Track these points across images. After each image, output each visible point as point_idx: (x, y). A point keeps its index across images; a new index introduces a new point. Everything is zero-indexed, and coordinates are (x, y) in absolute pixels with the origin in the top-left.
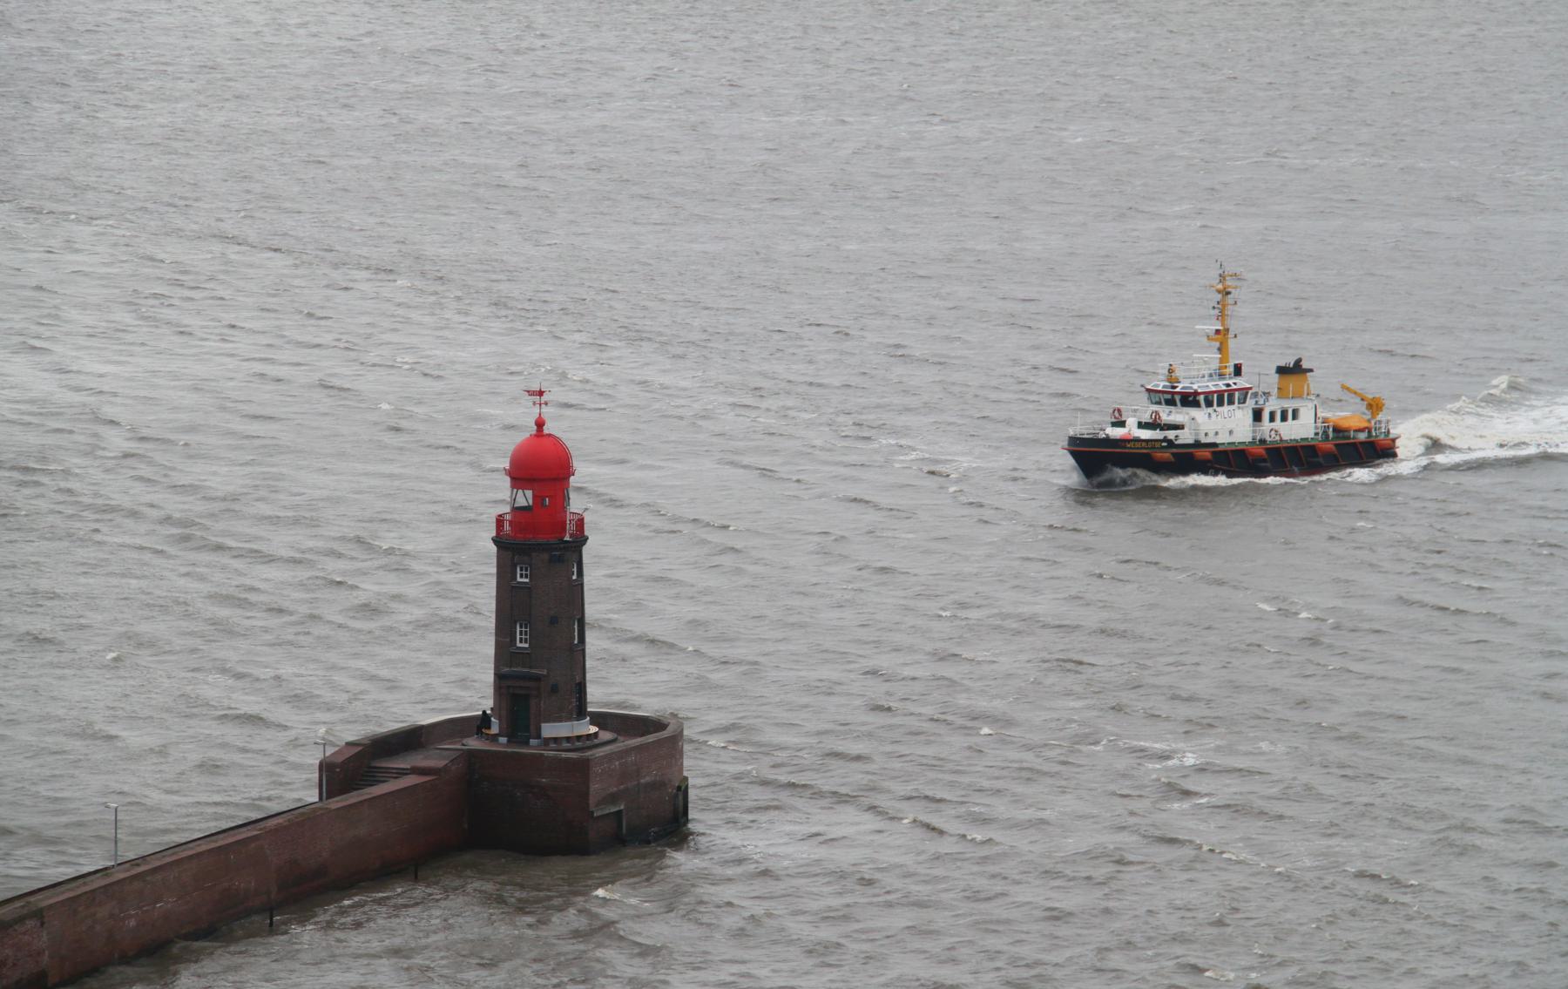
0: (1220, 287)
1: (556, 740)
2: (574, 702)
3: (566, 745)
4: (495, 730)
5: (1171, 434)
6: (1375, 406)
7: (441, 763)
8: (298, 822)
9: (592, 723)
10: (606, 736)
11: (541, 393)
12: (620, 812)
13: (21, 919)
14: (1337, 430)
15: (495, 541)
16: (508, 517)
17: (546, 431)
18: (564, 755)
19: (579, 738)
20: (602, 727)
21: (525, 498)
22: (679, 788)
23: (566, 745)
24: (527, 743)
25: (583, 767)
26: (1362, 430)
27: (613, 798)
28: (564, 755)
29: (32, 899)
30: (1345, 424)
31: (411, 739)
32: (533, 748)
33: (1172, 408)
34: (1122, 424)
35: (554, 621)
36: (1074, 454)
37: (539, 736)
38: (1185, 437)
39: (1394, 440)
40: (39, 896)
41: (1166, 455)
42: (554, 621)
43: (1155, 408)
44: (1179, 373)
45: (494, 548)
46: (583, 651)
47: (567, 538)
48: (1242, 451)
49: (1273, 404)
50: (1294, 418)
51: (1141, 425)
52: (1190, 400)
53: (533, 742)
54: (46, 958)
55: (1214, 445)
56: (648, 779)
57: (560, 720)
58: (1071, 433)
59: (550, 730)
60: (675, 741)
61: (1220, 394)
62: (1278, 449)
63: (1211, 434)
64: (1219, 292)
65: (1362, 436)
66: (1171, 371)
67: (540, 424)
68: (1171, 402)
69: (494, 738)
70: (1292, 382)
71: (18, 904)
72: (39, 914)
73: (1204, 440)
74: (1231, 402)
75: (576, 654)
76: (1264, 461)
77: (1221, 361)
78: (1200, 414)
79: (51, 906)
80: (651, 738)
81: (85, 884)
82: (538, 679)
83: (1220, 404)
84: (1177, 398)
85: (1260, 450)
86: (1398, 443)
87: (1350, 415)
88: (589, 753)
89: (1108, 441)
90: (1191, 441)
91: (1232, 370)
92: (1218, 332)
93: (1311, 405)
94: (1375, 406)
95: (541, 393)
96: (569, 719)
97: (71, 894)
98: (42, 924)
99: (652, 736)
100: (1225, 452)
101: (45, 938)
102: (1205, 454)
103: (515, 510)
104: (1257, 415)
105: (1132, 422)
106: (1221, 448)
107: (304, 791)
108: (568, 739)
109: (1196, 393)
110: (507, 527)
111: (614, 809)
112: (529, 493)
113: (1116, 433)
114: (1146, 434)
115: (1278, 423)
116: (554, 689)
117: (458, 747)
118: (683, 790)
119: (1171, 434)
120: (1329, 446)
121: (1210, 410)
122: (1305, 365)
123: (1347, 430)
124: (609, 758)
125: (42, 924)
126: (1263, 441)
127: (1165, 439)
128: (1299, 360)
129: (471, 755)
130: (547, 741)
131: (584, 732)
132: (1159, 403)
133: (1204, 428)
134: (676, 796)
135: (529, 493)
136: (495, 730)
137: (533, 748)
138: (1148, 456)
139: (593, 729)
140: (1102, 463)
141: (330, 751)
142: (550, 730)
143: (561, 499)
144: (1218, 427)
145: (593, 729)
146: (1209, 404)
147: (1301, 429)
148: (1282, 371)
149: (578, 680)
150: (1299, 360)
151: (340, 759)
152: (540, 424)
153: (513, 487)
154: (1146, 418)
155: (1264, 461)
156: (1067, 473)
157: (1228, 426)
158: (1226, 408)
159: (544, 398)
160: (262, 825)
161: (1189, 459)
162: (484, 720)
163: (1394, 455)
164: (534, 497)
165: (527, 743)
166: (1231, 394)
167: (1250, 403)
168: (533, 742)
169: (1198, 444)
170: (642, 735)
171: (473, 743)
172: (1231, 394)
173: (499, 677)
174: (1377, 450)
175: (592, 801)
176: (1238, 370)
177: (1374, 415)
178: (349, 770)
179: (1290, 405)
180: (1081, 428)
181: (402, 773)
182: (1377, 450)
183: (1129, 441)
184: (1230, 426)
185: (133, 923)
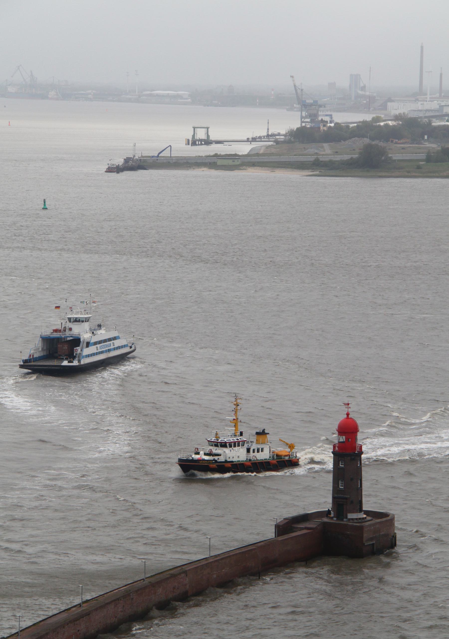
0: (235, 403)
1: (352, 519)
2: (358, 507)
3: (356, 521)
4: (332, 515)
5: (216, 458)
6: (291, 447)
7: (314, 526)
8: (266, 545)
9: (364, 514)
10: (369, 518)
11: (348, 404)
12: (373, 544)
13: (180, 574)
14: (277, 455)
15: (333, 453)
16: (337, 445)
17: (350, 416)
18: (355, 524)
19: (360, 519)
20: (367, 515)
21: (343, 439)
22: (393, 536)
23: (356, 521)
24: (342, 520)
25: (361, 529)
26: (286, 456)
27: (372, 539)
28: (355, 524)
29: (183, 567)
30: (280, 454)
31: (304, 518)
32: (345, 522)
33: (217, 448)
34: (198, 453)
35: (352, 480)
36: (180, 465)
37: (347, 518)
38: (222, 459)
39: (298, 459)
40: (186, 566)
41: (214, 466)
42: (352, 480)
43: (211, 448)
44: (219, 435)
45: (332, 455)
46: (361, 490)
47: (356, 452)
48: (243, 464)
49: (254, 446)
50: (262, 451)
51: (205, 454)
52: (224, 445)
53: (345, 520)
54: (188, 587)
55: (232, 462)
56: (383, 533)
57: (353, 512)
58: (179, 457)
59: (350, 516)
60: (391, 522)
61: (235, 443)
62: (256, 463)
63: (231, 458)
64: (235, 405)
65: (287, 458)
66: (217, 434)
67: (348, 414)
68: (216, 446)
69: (332, 518)
70: (261, 438)
71: (179, 569)
72: (185, 572)
73: (228, 460)
74: (239, 446)
75: (359, 490)
76: (251, 467)
77: (235, 430)
78: (227, 450)
79: (189, 570)
80: (384, 519)
81: (200, 563)
82: (346, 499)
83: (235, 446)
84: (219, 444)
85: (249, 464)
86: (299, 460)
87: (283, 450)
88: (364, 524)
89: (193, 461)
90: (224, 461)
91: (239, 434)
92: (234, 419)
93: (268, 447)
94: (291, 447)
95: (348, 404)
96: (356, 512)
97: (196, 566)
98: (187, 575)
99: (384, 518)
100: (236, 465)
101: (187, 580)
102: (229, 465)
103: (339, 442)
104: (248, 450)
105: (202, 453)
106: (235, 463)
107: (270, 533)
108: (356, 519)
109: (226, 443)
110: (337, 449)
111: (371, 543)
112: (344, 437)
113: (196, 457)
114: (207, 458)
115: (256, 453)
116: (352, 502)
117: (320, 521)
118: (394, 537)
119: (216, 458)
120: (275, 462)
121: (231, 449)
122: (266, 432)
123: (281, 456)
124: (370, 526)
125: (187, 575)
126: (250, 460)
127: (214, 460)
128: (264, 430)
129: (324, 524)
130: (350, 519)
131: (362, 517)
132: (212, 446)
133: (228, 455)
134: (392, 539)
135: (344, 437)
136: (332, 515)
137: (345, 522)
138: (208, 466)
139: (365, 516)
140: (191, 469)
141: (278, 521)
142: (350, 516)
143: (355, 439)
144: (234, 455)
145: (365, 516)
146: (230, 446)
147: (264, 455)
148: (258, 434)
149: (360, 499)
150: (264, 430)
151: (282, 524)
152: (348, 414)
153: (339, 435)
154: (207, 452)
155: (251, 467)
156: (176, 471)
157: (238, 455)
158: (237, 448)
159: (350, 406)
160: (256, 545)
161: (222, 467)
162: (329, 512)
163: (298, 465)
164: (346, 438)
165: (342, 520)
166: (239, 443)
167: (246, 446)
168: (345, 520)
169: (226, 462)
170: (381, 518)
171: (325, 520)
172: (239, 443)
173: (334, 498)
174: (294, 463)
175: (364, 540)
176: (241, 434)
177: (291, 451)
178: (285, 527)
179: (260, 446)
180: (183, 456)
181: (302, 529)
182: (293, 463)
183: (201, 460)
184: (238, 455)
185: (215, 576)
